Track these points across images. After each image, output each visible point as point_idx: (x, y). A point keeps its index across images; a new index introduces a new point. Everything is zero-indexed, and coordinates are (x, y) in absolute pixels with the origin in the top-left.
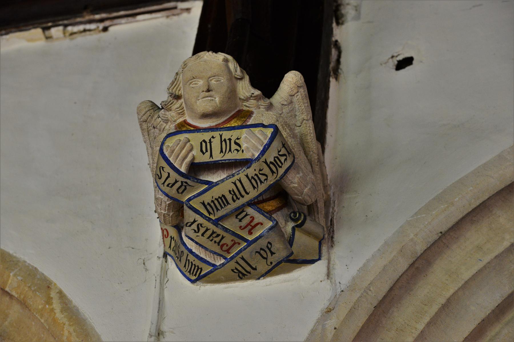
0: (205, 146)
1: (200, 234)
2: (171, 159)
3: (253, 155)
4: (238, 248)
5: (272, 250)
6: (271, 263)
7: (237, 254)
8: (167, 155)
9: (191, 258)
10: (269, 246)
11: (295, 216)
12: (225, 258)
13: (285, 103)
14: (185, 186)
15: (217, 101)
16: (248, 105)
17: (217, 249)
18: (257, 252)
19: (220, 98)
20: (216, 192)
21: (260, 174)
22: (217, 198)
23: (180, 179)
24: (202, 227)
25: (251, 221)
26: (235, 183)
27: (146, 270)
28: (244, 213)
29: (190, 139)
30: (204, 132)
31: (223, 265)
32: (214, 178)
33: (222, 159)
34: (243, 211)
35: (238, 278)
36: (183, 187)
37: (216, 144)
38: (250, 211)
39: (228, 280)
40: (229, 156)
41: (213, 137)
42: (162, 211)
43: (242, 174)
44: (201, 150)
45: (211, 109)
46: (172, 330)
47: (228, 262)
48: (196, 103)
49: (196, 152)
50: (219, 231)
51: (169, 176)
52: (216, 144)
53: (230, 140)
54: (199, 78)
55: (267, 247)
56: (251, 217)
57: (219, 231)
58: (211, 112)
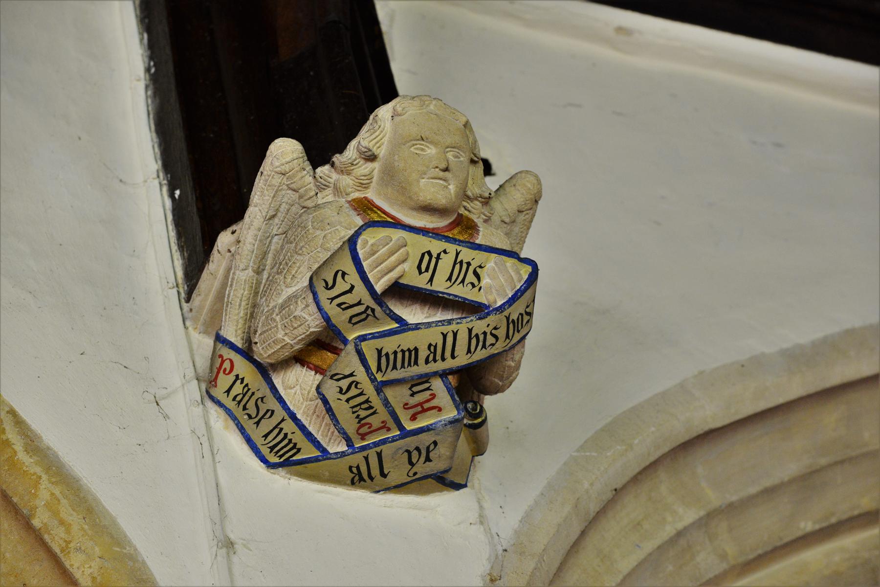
0: (427, 263)
1: (344, 397)
2: (365, 264)
3: (495, 302)
4: (382, 435)
5: (431, 455)
6: (415, 474)
7: (376, 444)
8: (361, 256)
9: (289, 426)
10: (432, 447)
11: (475, 409)
12: (349, 442)
13: (507, 220)
14: (368, 315)
15: (452, 192)
16: (470, 208)
17: (350, 425)
18: (407, 451)
19: (457, 187)
20: (407, 340)
21: (492, 334)
22: (405, 349)
23: (368, 301)
24: (356, 387)
25: (428, 401)
26: (445, 336)
27: (166, 417)
28: (427, 385)
29: (409, 243)
30: (434, 238)
31: (343, 454)
32: (413, 314)
33: (446, 291)
34: (427, 382)
35: (349, 482)
36: (364, 316)
37: (446, 263)
38: (437, 384)
39: (334, 480)
40: (458, 291)
41: (445, 252)
42: (286, 338)
43: (464, 325)
44: (419, 267)
45: (444, 201)
46: (245, 542)
47: (352, 453)
48: (418, 181)
49: (410, 267)
50: (376, 402)
51: (350, 291)
52: (446, 263)
53: (469, 264)
54: (431, 143)
55: (428, 448)
56: (431, 395)
57: (376, 402)
58: (441, 207)
